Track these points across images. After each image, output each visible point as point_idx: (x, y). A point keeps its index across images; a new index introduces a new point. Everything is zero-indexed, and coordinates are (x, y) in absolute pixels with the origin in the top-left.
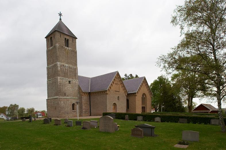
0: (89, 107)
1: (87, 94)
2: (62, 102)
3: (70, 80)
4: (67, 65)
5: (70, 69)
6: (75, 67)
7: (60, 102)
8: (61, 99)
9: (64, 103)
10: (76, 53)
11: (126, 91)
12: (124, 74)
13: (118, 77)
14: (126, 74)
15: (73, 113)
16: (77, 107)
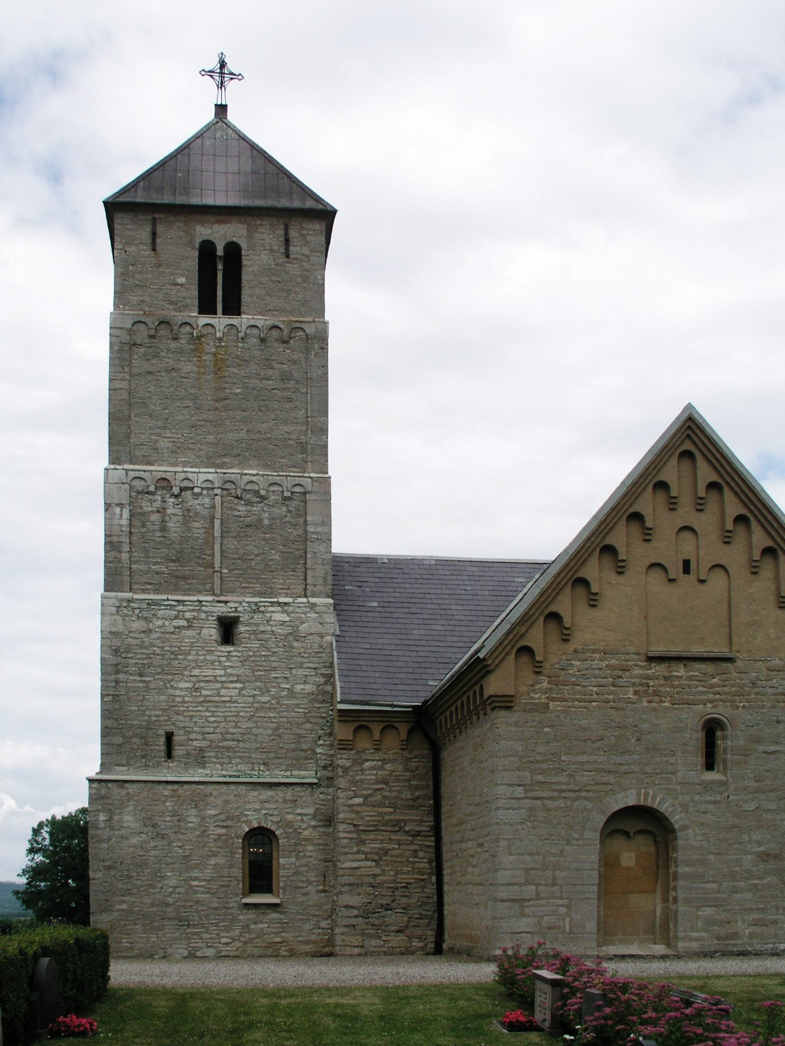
1: (404, 729)
2: (129, 819)
3: (237, 603)
4: (203, 475)
5: (242, 508)
6: (289, 479)
8: (116, 791)
9: (150, 822)
13: (706, 474)
15: (246, 916)
16: (481, 841)
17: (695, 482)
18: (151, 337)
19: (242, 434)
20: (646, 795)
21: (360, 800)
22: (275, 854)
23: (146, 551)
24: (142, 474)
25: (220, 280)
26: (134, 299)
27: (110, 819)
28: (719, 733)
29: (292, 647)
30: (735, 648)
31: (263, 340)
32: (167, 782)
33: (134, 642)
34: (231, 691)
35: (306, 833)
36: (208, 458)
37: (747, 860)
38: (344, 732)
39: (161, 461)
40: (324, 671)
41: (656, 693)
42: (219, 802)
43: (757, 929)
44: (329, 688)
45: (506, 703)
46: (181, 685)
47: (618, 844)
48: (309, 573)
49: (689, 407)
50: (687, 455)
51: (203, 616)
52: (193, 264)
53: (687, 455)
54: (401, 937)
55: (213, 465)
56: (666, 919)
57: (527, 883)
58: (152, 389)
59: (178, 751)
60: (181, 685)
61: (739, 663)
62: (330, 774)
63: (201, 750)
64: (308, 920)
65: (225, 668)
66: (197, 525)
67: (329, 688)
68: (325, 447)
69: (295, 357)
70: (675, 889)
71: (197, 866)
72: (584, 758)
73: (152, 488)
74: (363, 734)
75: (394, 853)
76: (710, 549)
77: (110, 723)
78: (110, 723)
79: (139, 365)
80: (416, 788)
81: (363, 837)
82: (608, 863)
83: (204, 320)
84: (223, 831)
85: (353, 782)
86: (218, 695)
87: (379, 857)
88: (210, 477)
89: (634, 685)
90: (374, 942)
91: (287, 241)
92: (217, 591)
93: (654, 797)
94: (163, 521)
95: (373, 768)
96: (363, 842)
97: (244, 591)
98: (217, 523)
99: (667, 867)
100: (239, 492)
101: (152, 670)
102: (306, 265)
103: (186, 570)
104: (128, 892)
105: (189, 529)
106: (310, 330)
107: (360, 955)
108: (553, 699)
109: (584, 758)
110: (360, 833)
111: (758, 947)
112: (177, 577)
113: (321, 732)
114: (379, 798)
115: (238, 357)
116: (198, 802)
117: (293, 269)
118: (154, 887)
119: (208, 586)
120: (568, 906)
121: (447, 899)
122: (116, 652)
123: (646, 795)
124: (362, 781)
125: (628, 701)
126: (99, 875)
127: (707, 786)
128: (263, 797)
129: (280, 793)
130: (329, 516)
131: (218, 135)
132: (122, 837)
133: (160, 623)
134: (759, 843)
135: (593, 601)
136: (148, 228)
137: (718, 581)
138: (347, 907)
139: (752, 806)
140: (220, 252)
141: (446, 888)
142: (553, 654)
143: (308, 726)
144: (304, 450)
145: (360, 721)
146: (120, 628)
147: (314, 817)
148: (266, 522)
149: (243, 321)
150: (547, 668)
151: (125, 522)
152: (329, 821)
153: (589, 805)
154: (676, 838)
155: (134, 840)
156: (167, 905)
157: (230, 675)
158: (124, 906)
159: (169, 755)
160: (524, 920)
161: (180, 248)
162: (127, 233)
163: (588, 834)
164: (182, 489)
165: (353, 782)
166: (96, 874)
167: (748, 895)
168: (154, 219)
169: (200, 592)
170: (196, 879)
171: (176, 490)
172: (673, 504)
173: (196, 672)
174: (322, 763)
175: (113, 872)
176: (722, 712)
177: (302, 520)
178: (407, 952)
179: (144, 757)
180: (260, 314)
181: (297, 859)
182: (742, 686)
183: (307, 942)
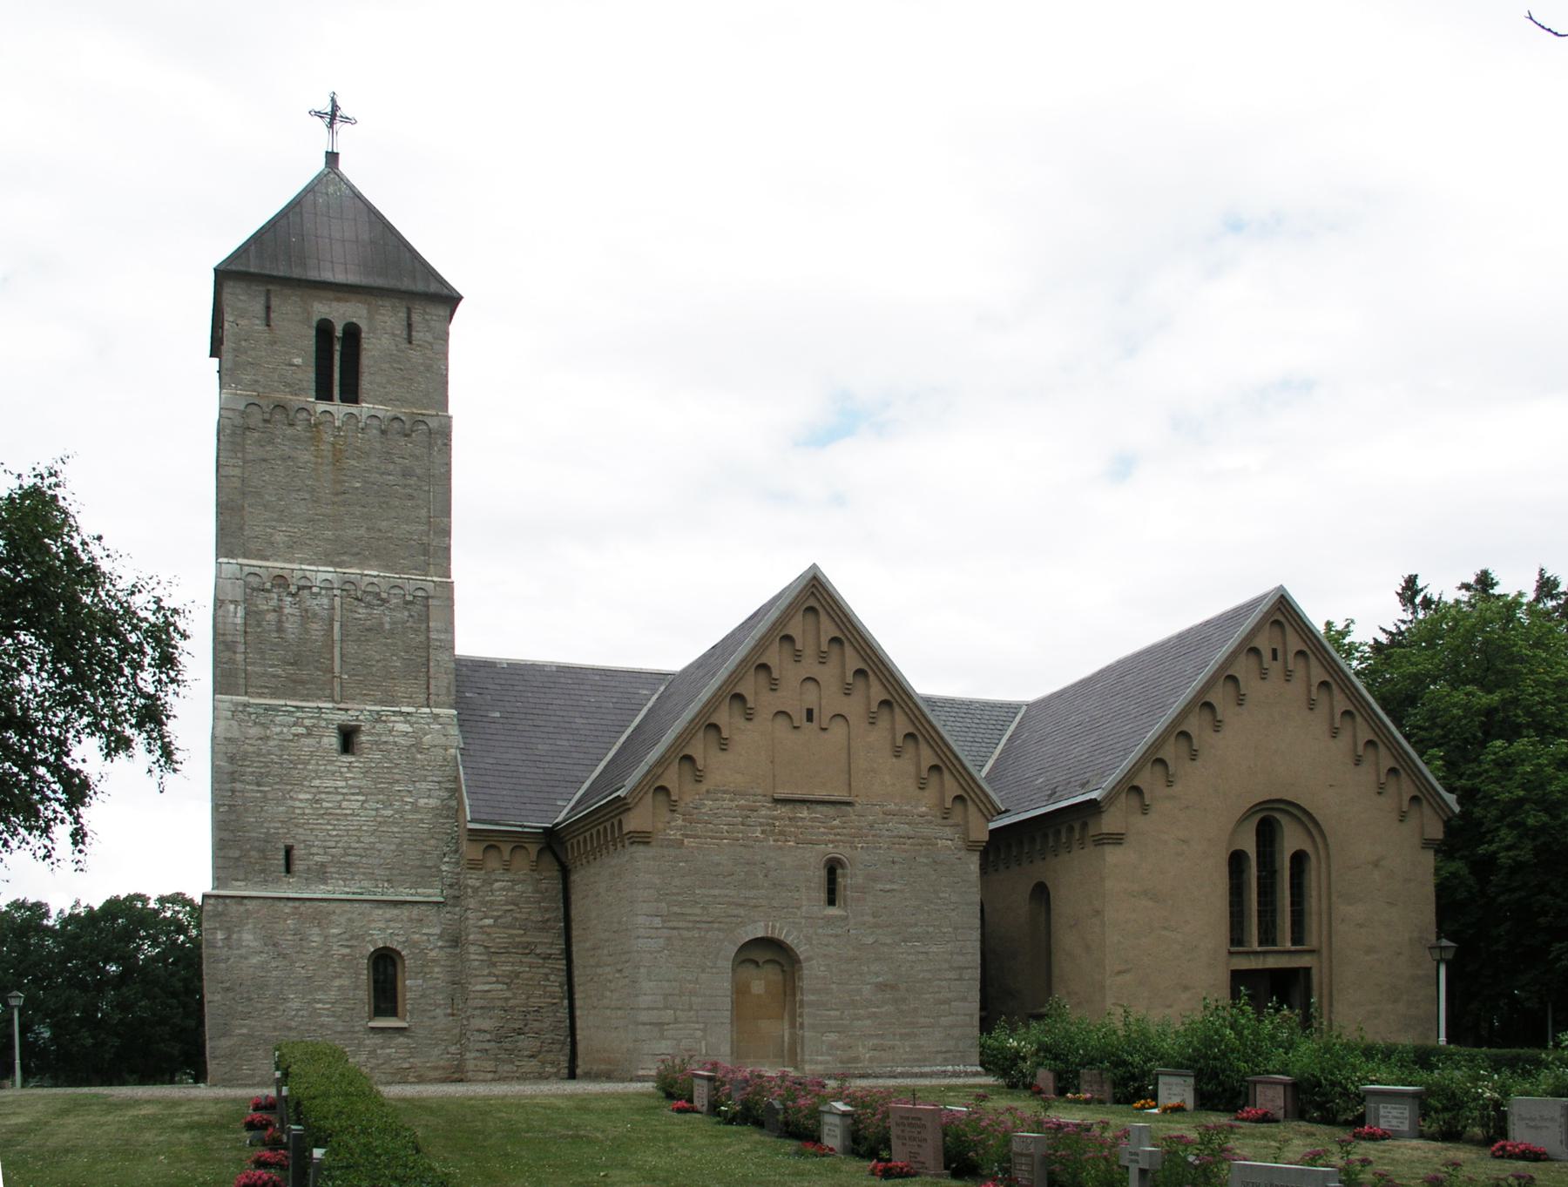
0: (556, 984)
1: (533, 849)
3: (358, 712)
4: (323, 573)
5: (362, 611)
6: (413, 581)
7: (229, 931)
8: (234, 908)
9: (271, 941)
10: (440, 437)
11: (969, 795)
12: (1398, 584)
14: (1411, 581)
17: (818, 638)
18: (266, 421)
19: (362, 532)
20: (773, 927)
21: (491, 921)
22: (400, 975)
23: (262, 652)
24: (257, 570)
25: (338, 363)
26: (247, 378)
27: (228, 938)
28: (839, 871)
29: (414, 759)
30: (854, 792)
31: (383, 432)
32: (289, 899)
33: (251, 749)
34: (353, 804)
35: (433, 954)
36: (327, 555)
37: (867, 989)
38: (473, 851)
39: (275, 556)
40: (448, 785)
41: (782, 833)
42: (343, 920)
43: (876, 1054)
44: (454, 803)
45: (643, 838)
46: (301, 796)
47: (749, 972)
48: (432, 682)
49: (814, 566)
50: (811, 610)
51: (323, 724)
52: (310, 343)
53: (811, 610)
54: (534, 1062)
55: (331, 564)
56: (793, 1043)
57: (666, 1008)
58: (267, 478)
59: (298, 866)
60: (301, 796)
61: (858, 807)
62: (457, 893)
63: (323, 865)
64: (437, 1045)
65: (346, 780)
66: (315, 626)
67: (454, 803)
68: (448, 549)
69: (417, 452)
70: (801, 1016)
71: (320, 988)
72: (716, 892)
73: (268, 585)
74: (493, 853)
75: (526, 976)
76: (830, 699)
77: (226, 835)
78: (226, 835)
79: (253, 451)
80: (546, 910)
81: (494, 959)
82: (740, 991)
83: (322, 406)
84: (348, 951)
85: (484, 903)
86: (340, 807)
87: (511, 979)
88: (329, 576)
89: (761, 824)
90: (507, 1067)
91: (410, 326)
92: (337, 698)
93: (781, 929)
94: (280, 621)
95: (503, 889)
96: (494, 965)
97: (365, 698)
98: (337, 626)
99: (794, 995)
100: (359, 594)
101: (270, 780)
102: (429, 353)
103: (304, 674)
104: (248, 1015)
105: (307, 631)
106: (433, 423)
107: (493, 1080)
108: (687, 836)
109: (716, 892)
110: (492, 955)
111: (877, 1070)
112: (294, 681)
113: (446, 849)
114: (509, 919)
115: (357, 449)
116: (320, 919)
117: (415, 356)
118: (275, 1009)
119: (327, 692)
120: (704, 1030)
121: (579, 1023)
122: (232, 759)
123: (773, 927)
124: (492, 902)
125: (756, 840)
126: (218, 997)
127: (829, 921)
128: (388, 916)
129: (405, 912)
130: (452, 623)
131: (331, 190)
132: (241, 957)
133: (278, 729)
134: (877, 974)
135: (724, 744)
136: (262, 300)
137: (838, 729)
138: (479, 1030)
139: (870, 940)
140: (339, 333)
141: (578, 1013)
142: (687, 793)
143: (433, 842)
144: (426, 552)
145: (488, 840)
146: (236, 734)
147: (441, 937)
148: (387, 626)
149: (365, 408)
150: (681, 807)
151: (239, 621)
152: (455, 941)
153: (721, 936)
154: (801, 968)
155: (254, 960)
156: (290, 1029)
157: (352, 787)
158: (244, 1031)
159: (288, 870)
160: (664, 1043)
161: (296, 325)
162: (240, 305)
163: (720, 963)
164: (299, 588)
165: (484, 903)
166: (213, 998)
167: (868, 1022)
168: (268, 292)
169: (319, 698)
170: (320, 1001)
171: (293, 589)
172: (797, 656)
173: (317, 783)
174: (448, 881)
175: (231, 995)
176: (842, 852)
177: (424, 626)
178: (541, 1077)
179: (263, 871)
180: (381, 403)
181: (425, 980)
182: (861, 828)
183: (435, 1068)
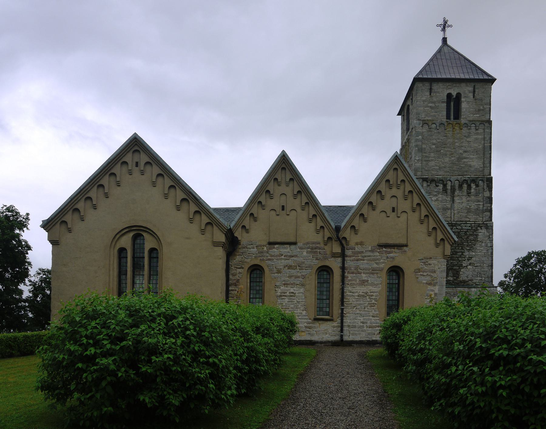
13: (401, 177)
50: (396, 169)
53: (283, 169)
137: (404, 215)
